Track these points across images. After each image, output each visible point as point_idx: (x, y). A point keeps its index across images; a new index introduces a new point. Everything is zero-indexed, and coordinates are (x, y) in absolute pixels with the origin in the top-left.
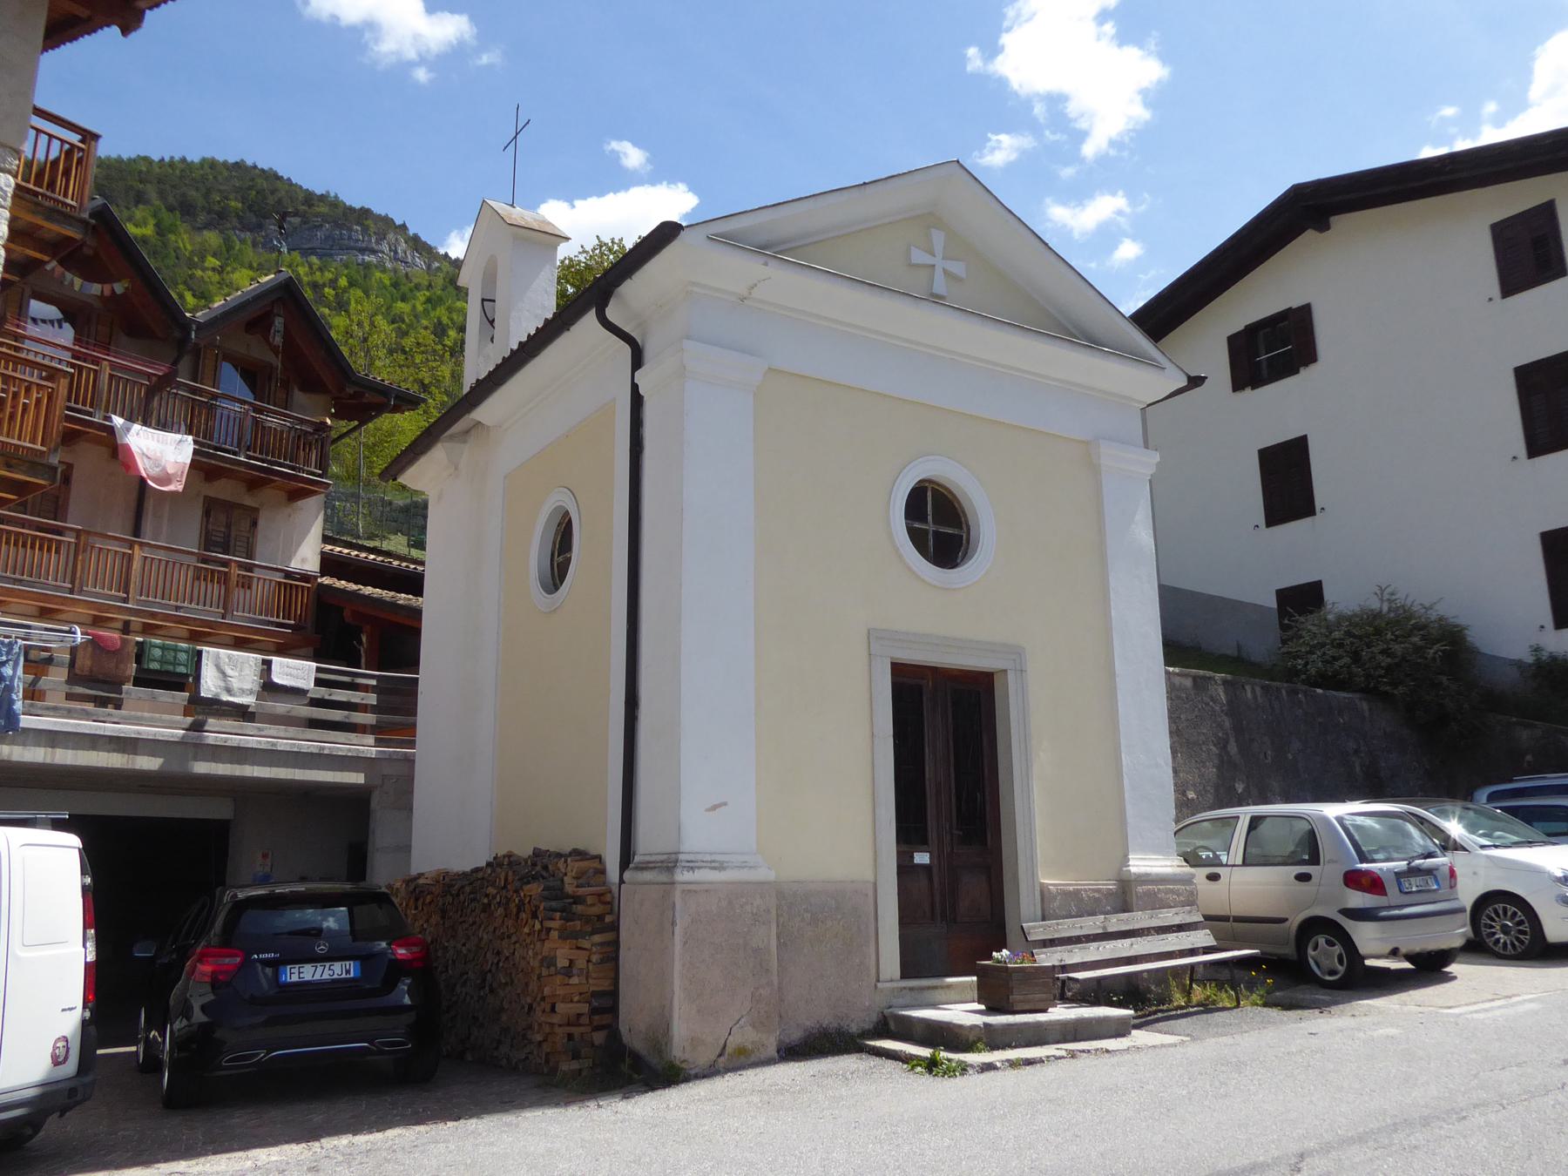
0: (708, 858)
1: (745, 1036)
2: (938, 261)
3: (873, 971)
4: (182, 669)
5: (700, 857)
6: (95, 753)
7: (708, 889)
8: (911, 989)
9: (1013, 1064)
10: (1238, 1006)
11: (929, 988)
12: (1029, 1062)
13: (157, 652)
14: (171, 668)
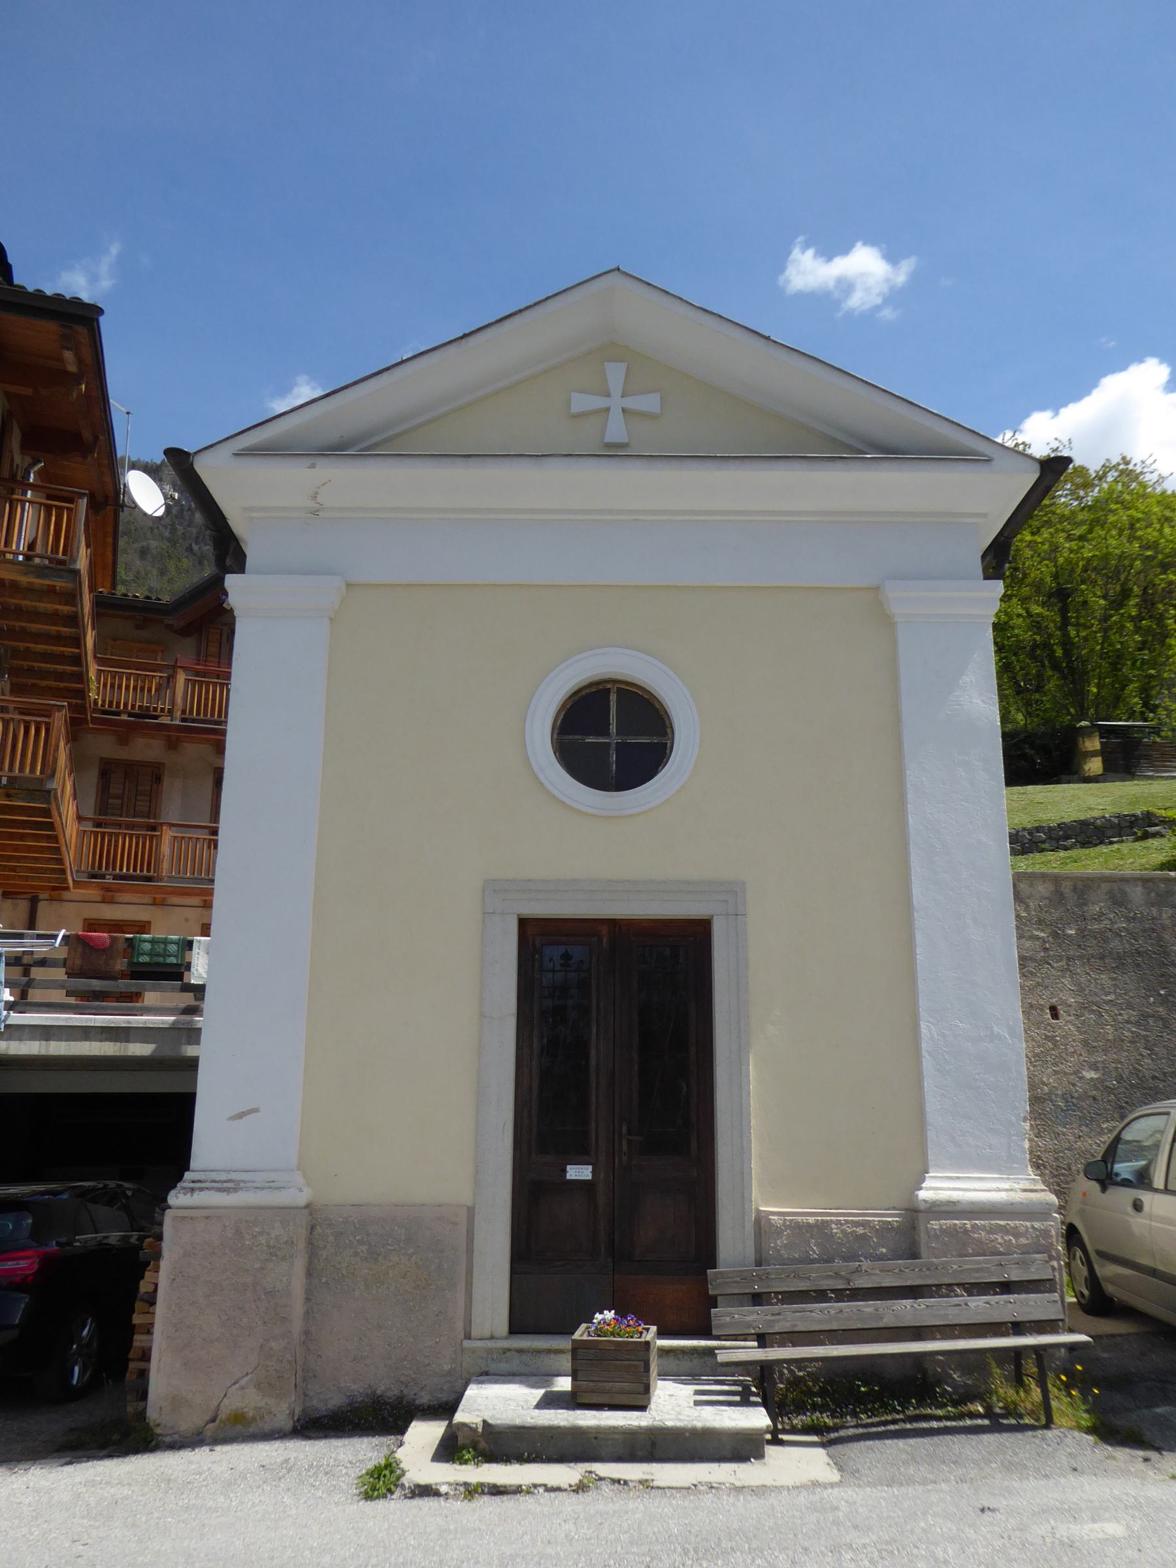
0: (224, 1177)
1: (247, 1400)
2: (616, 403)
3: (460, 1325)
4: (173, 960)
5: (214, 1176)
6: (88, 1043)
7: (210, 1214)
8: (520, 1351)
9: (472, 1491)
10: (1047, 1426)
11: (549, 1351)
12: (497, 1491)
13: (147, 947)
14: (161, 960)
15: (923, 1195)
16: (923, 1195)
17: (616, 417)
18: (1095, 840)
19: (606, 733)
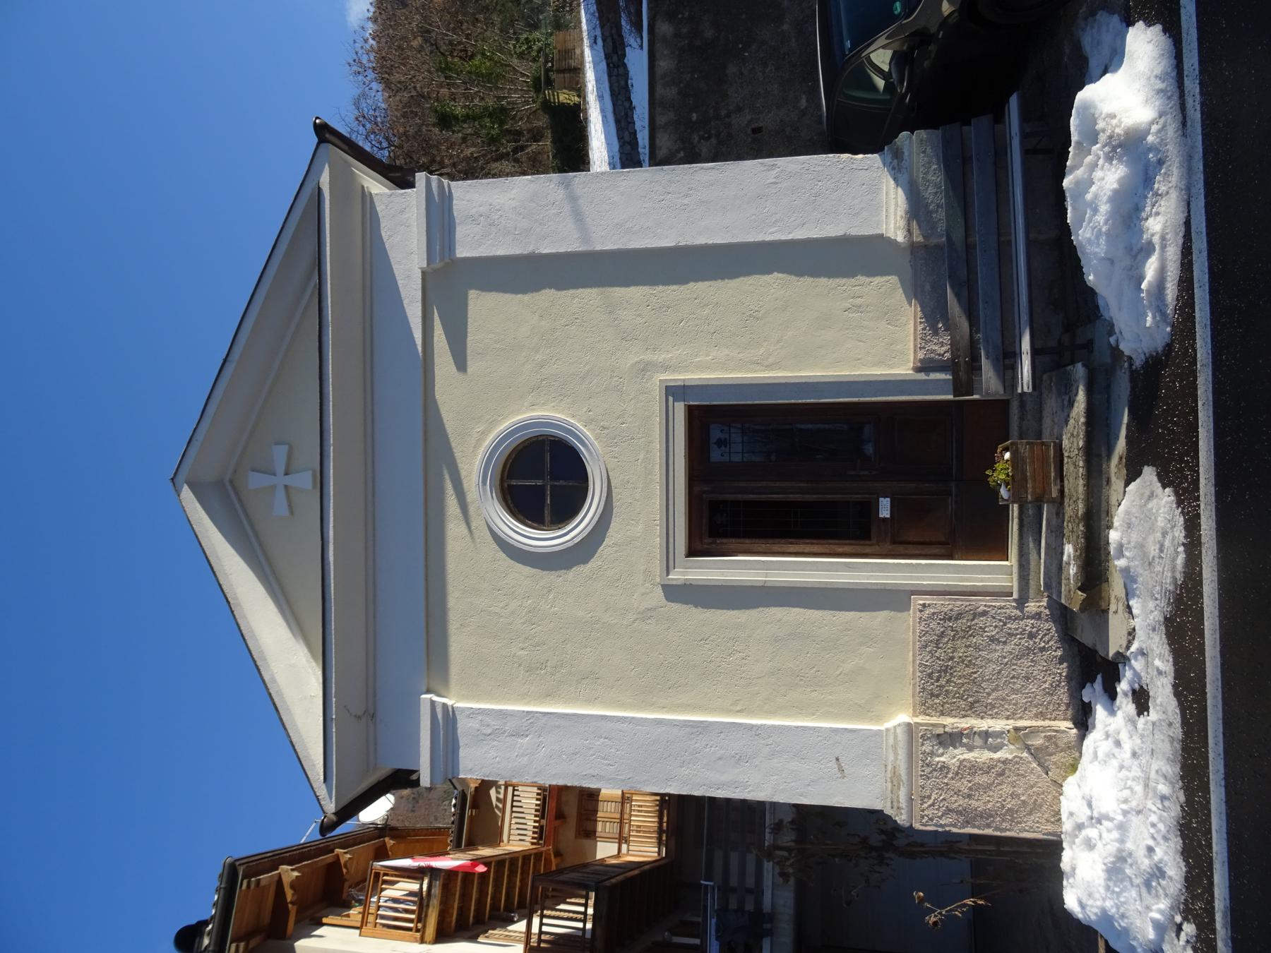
15: (900, 237)
16: (900, 237)
17: (292, 480)
18: (621, 71)
19: (542, 488)
